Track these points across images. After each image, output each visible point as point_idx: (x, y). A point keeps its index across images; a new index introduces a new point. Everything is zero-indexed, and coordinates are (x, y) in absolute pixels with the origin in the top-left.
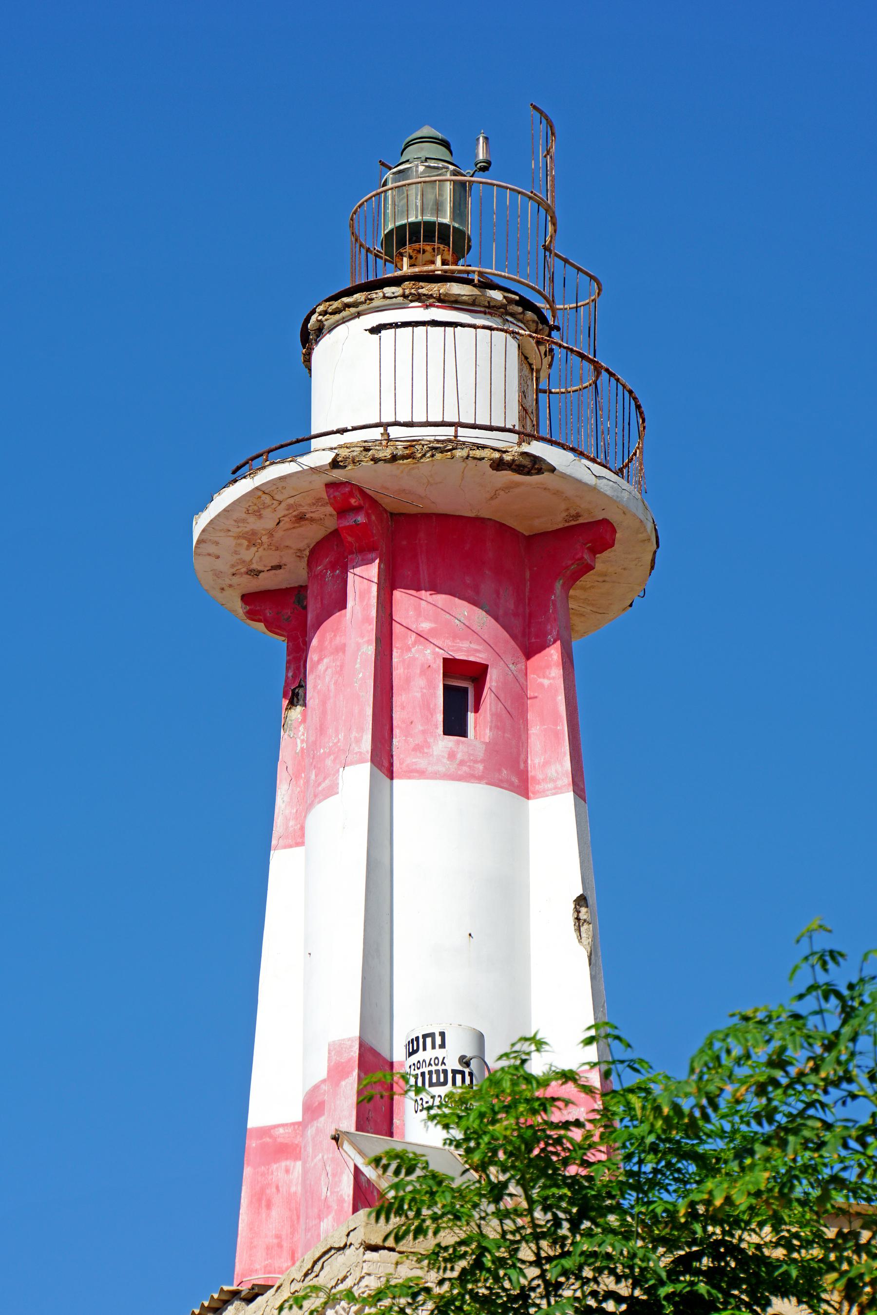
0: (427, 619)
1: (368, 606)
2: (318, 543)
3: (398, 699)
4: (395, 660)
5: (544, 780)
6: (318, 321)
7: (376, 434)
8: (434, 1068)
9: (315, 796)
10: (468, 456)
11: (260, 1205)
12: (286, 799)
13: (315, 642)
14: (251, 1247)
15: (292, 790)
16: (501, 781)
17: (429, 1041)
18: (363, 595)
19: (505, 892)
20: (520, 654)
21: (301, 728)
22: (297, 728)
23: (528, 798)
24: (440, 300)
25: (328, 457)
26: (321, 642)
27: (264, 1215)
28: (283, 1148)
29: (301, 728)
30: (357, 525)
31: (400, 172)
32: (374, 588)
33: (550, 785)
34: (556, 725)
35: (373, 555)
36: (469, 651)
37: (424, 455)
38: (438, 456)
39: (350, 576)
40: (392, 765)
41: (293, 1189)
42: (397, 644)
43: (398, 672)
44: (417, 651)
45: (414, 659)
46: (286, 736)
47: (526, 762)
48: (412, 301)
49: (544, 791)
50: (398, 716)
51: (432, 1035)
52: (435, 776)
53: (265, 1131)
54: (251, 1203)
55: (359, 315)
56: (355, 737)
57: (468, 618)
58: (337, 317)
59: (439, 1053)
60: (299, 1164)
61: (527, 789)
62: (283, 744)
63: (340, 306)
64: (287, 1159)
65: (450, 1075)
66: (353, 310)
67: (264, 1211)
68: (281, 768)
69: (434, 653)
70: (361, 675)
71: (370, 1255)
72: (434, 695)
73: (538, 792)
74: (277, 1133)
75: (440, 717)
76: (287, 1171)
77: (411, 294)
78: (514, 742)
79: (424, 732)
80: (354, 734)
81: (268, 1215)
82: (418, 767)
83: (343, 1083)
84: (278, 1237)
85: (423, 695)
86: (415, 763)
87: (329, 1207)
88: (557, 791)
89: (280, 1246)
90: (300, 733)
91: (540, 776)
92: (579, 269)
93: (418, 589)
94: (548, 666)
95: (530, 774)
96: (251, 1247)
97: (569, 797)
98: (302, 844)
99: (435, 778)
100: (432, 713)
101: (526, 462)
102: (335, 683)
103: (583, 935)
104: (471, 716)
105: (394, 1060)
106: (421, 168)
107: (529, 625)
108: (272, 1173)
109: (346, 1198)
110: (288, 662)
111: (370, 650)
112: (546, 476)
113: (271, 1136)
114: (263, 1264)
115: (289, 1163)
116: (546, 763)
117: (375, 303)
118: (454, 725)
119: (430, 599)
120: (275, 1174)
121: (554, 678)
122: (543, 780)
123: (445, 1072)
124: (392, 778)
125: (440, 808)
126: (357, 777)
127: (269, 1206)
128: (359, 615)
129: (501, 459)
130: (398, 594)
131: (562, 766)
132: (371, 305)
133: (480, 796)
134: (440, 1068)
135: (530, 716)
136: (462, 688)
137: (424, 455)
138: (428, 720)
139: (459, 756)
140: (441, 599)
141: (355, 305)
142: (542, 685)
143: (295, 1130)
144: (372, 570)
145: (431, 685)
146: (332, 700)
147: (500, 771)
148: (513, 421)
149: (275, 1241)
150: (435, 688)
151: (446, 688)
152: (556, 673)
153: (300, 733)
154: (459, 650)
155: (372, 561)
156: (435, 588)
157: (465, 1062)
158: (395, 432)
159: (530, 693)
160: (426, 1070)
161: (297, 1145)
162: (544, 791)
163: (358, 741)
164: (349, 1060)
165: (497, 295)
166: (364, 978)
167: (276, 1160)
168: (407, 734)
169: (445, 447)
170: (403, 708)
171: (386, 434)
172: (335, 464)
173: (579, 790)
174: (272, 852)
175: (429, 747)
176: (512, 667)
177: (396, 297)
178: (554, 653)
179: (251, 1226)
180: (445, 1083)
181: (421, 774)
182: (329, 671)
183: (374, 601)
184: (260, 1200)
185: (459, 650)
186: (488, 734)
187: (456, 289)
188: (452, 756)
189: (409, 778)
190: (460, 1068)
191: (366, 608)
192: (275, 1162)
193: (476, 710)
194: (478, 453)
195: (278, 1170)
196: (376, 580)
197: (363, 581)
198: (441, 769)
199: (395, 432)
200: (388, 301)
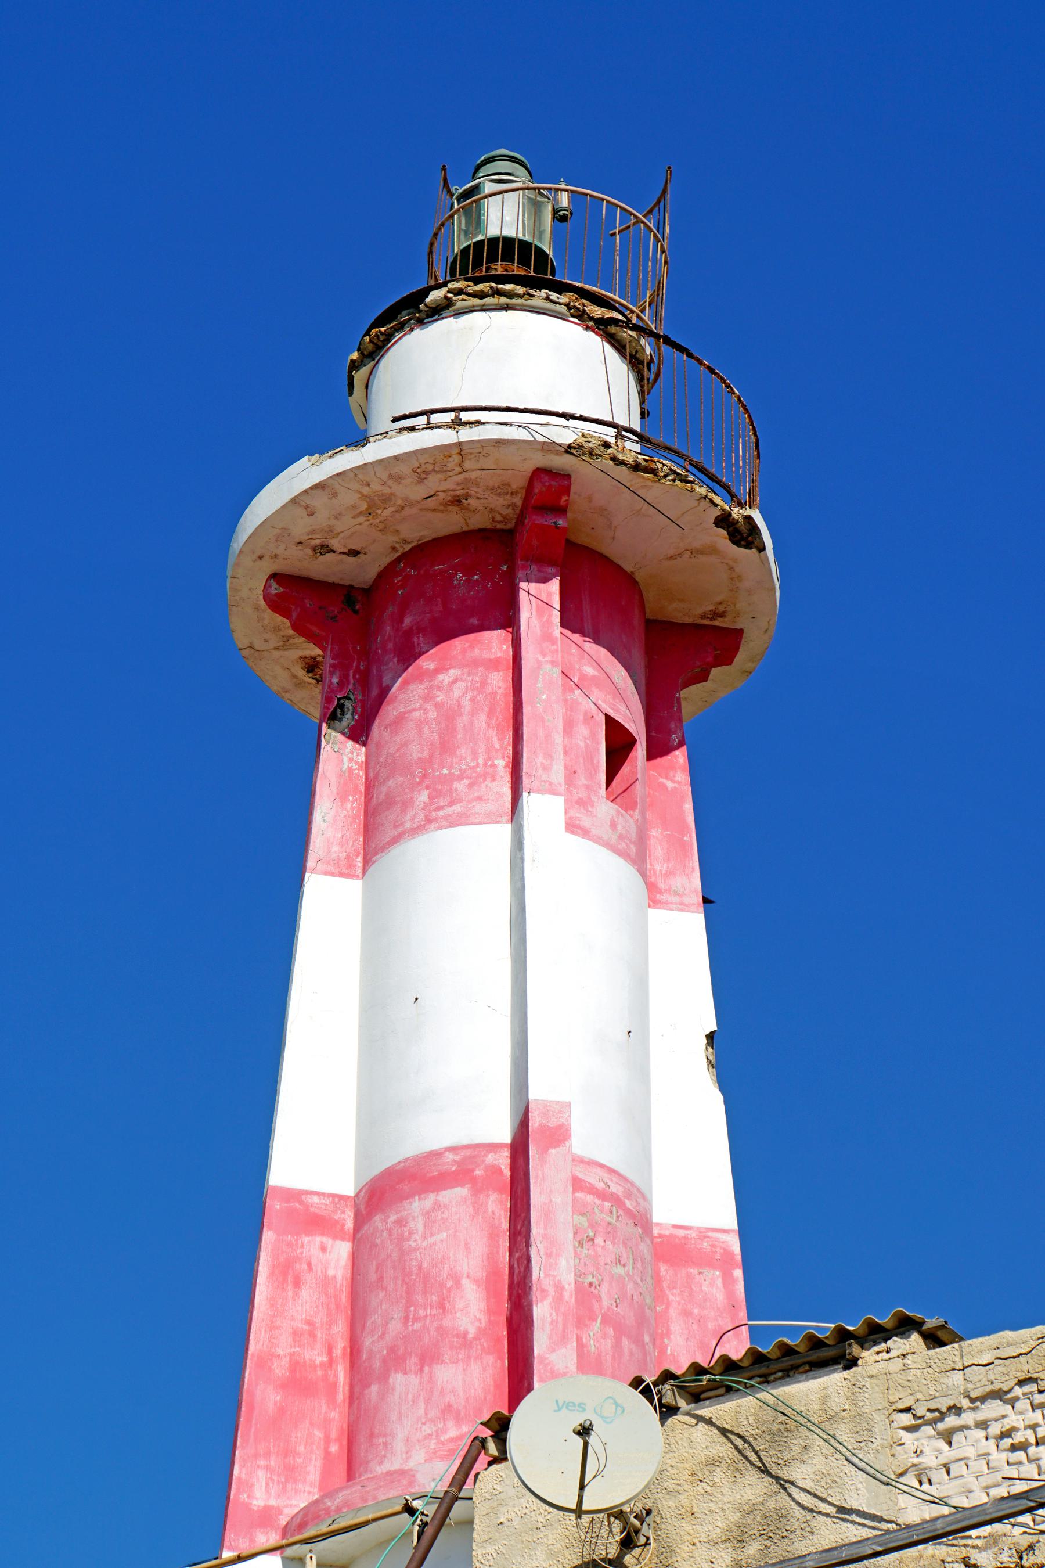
2: (435, 541)
5: (668, 890)
6: (446, 297)
10: (706, 496)
11: (285, 1281)
12: (329, 818)
15: (337, 812)
27: (290, 1294)
28: (311, 1217)
30: (557, 527)
33: (676, 899)
34: (684, 835)
35: (552, 570)
37: (665, 476)
38: (678, 483)
41: (331, 1272)
46: (328, 748)
48: (572, 316)
49: (667, 903)
52: (598, 840)
53: (292, 1195)
54: (271, 1275)
55: (507, 308)
56: (542, 763)
58: (477, 301)
63: (486, 290)
64: (323, 1234)
66: (504, 300)
70: (544, 697)
73: (659, 902)
74: (310, 1201)
76: (323, 1249)
77: (575, 307)
79: (588, 787)
81: (296, 1295)
82: (582, 824)
83: (553, 1151)
85: (587, 746)
88: (683, 907)
89: (312, 1335)
90: (347, 750)
93: (574, 631)
94: (673, 768)
96: (272, 1327)
99: (600, 844)
100: (596, 769)
101: (743, 527)
108: (302, 1247)
109: (567, 1286)
113: (301, 1202)
114: (288, 1351)
115: (327, 1241)
116: (669, 874)
117: (533, 302)
120: (306, 1247)
121: (679, 783)
122: (666, 890)
127: (297, 1283)
132: (529, 302)
137: (665, 476)
138: (591, 776)
141: (510, 295)
142: (665, 786)
143: (333, 1202)
145: (593, 736)
146: (465, 718)
149: (306, 1327)
153: (347, 750)
154: (617, 710)
155: (545, 580)
161: (337, 1222)
162: (667, 903)
167: (308, 1234)
169: (687, 476)
174: (307, 875)
177: (560, 304)
179: (272, 1302)
184: (285, 1274)
192: (307, 1235)
200: (550, 305)
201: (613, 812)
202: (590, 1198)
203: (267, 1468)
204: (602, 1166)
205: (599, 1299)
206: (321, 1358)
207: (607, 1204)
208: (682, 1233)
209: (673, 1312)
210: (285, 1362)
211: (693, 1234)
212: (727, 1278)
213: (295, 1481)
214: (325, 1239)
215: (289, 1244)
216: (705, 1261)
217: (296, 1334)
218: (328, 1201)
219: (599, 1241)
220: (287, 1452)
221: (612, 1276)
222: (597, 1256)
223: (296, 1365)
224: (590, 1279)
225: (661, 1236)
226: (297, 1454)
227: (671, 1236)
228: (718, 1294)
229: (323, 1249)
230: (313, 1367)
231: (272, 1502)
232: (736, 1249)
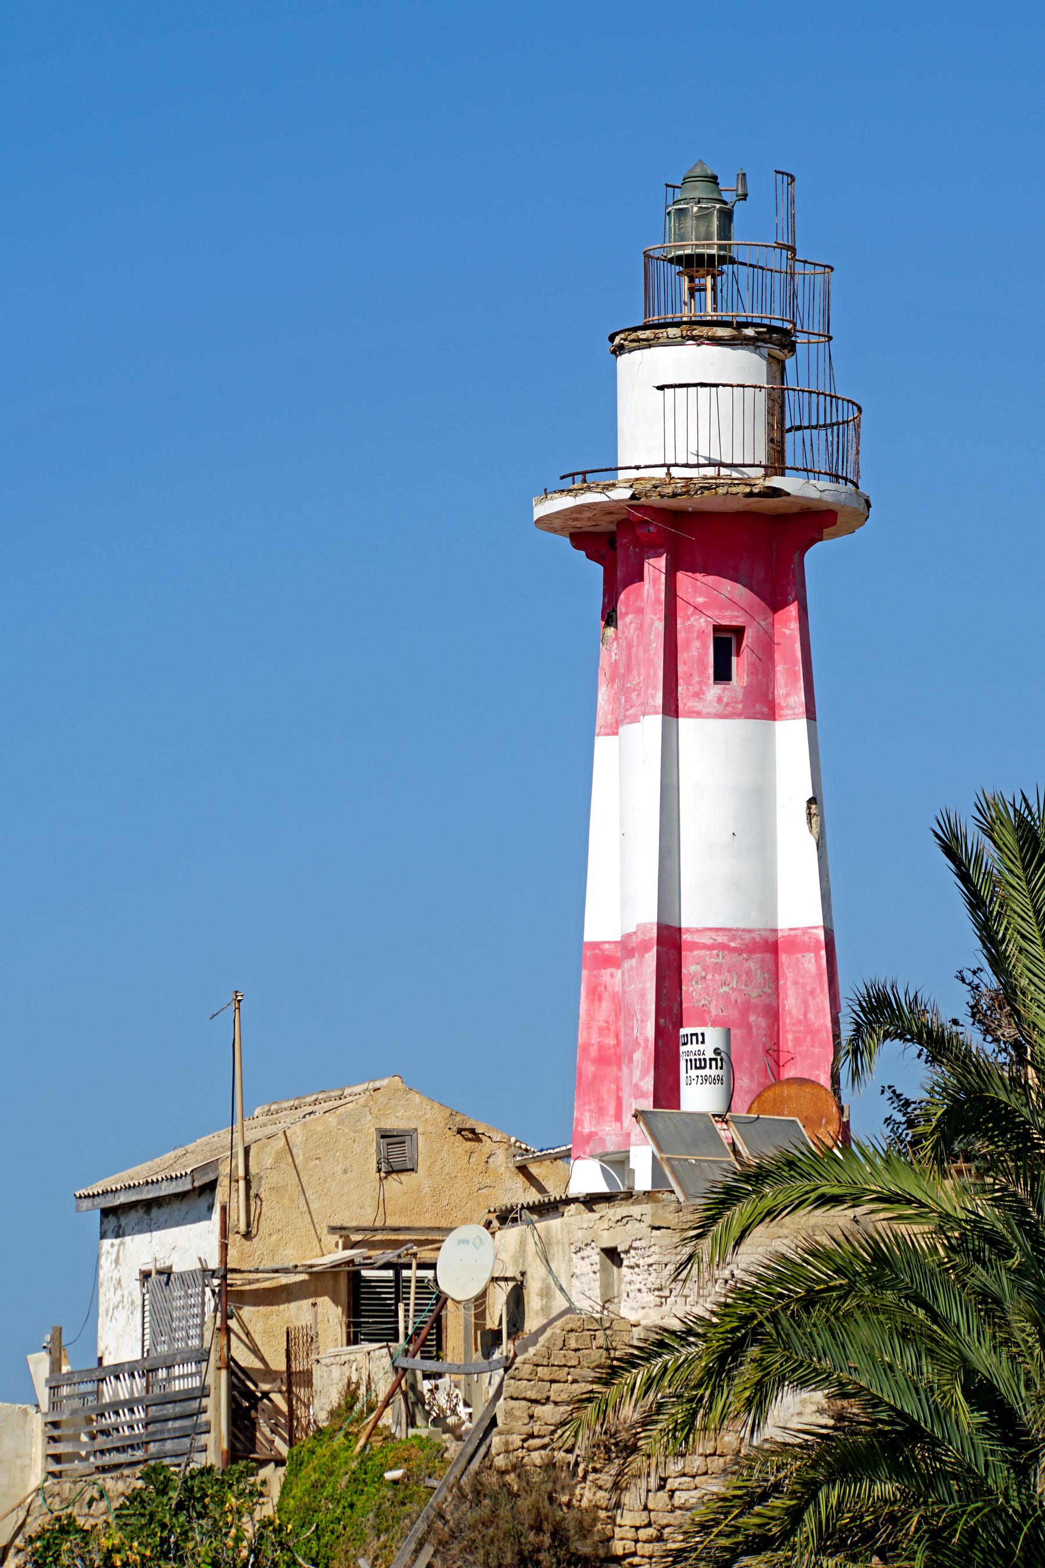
0: (701, 595)
1: (659, 589)
3: (682, 657)
4: (679, 626)
7: (661, 473)
8: (697, 1057)
13: (622, 596)
14: (589, 1028)
16: (755, 713)
17: (694, 1038)
18: (655, 581)
21: (615, 644)
22: (612, 644)
23: (775, 720)
24: (708, 339)
25: (627, 494)
26: (627, 598)
29: (615, 644)
31: (680, 209)
32: (663, 577)
33: (790, 712)
34: (795, 666)
35: (662, 550)
36: (732, 618)
38: (706, 493)
39: (646, 565)
40: (677, 706)
41: (616, 989)
43: (681, 636)
44: (695, 620)
45: (692, 626)
47: (773, 693)
50: (681, 669)
51: (696, 1035)
52: (709, 716)
53: (596, 945)
54: (587, 996)
55: (650, 346)
57: (730, 592)
59: (701, 1047)
60: (620, 971)
61: (774, 713)
62: (602, 655)
65: (708, 1062)
67: (596, 1002)
68: (601, 674)
69: (706, 621)
71: (655, 1233)
72: (707, 654)
75: (711, 671)
76: (612, 976)
78: (764, 681)
79: (700, 683)
80: (650, 691)
81: (600, 1006)
83: (647, 955)
84: (607, 1022)
85: (699, 654)
86: (694, 706)
87: (638, 1044)
88: (795, 716)
89: (608, 1029)
91: (783, 704)
92: (815, 264)
93: (694, 572)
94: (789, 620)
95: (777, 701)
96: (589, 1028)
98: (616, 734)
100: (706, 667)
101: (770, 491)
102: (638, 636)
103: (814, 826)
104: (734, 659)
105: (683, 926)
106: (695, 209)
107: (714, 1219)
111: (660, 626)
112: (784, 498)
113: (600, 949)
116: (788, 695)
117: (661, 341)
118: (722, 674)
119: (703, 579)
124: (677, 717)
125: (709, 741)
126: (654, 722)
127: (600, 999)
130: (680, 575)
133: (739, 729)
134: (702, 1057)
136: (726, 643)
139: (725, 700)
140: (711, 579)
142: (784, 633)
144: (662, 562)
145: (704, 647)
147: (754, 706)
148: (762, 458)
150: (707, 648)
152: (795, 625)
155: (660, 556)
157: (717, 1051)
158: (676, 472)
159: (776, 640)
160: (693, 1058)
163: (653, 696)
164: (651, 939)
165: (750, 332)
166: (660, 878)
167: (605, 968)
170: (685, 664)
171: (668, 474)
172: (633, 497)
173: (811, 714)
175: (704, 694)
176: (763, 623)
178: (793, 610)
181: (698, 714)
182: (633, 625)
185: (724, 617)
188: (720, 700)
189: (690, 717)
190: (714, 1056)
193: (738, 655)
194: (734, 490)
195: (606, 974)
196: (664, 570)
198: (713, 710)
199: (676, 472)
201: (719, 691)
202: (702, 953)
203: (590, 1110)
204: (711, 929)
205: (709, 1012)
206: (613, 1042)
207: (714, 952)
208: (793, 933)
209: (789, 983)
210: (596, 1047)
211: (799, 932)
212: (818, 957)
214: (612, 970)
215: (596, 976)
216: (805, 948)
217: (600, 1029)
218: (613, 946)
219: (710, 977)
220: (599, 1100)
221: (718, 995)
222: (708, 987)
223: (601, 1048)
224: (703, 1002)
225: (783, 937)
226: (603, 1100)
227: (789, 936)
229: (612, 976)
230: (610, 1048)
231: (593, 1129)
232: (822, 938)
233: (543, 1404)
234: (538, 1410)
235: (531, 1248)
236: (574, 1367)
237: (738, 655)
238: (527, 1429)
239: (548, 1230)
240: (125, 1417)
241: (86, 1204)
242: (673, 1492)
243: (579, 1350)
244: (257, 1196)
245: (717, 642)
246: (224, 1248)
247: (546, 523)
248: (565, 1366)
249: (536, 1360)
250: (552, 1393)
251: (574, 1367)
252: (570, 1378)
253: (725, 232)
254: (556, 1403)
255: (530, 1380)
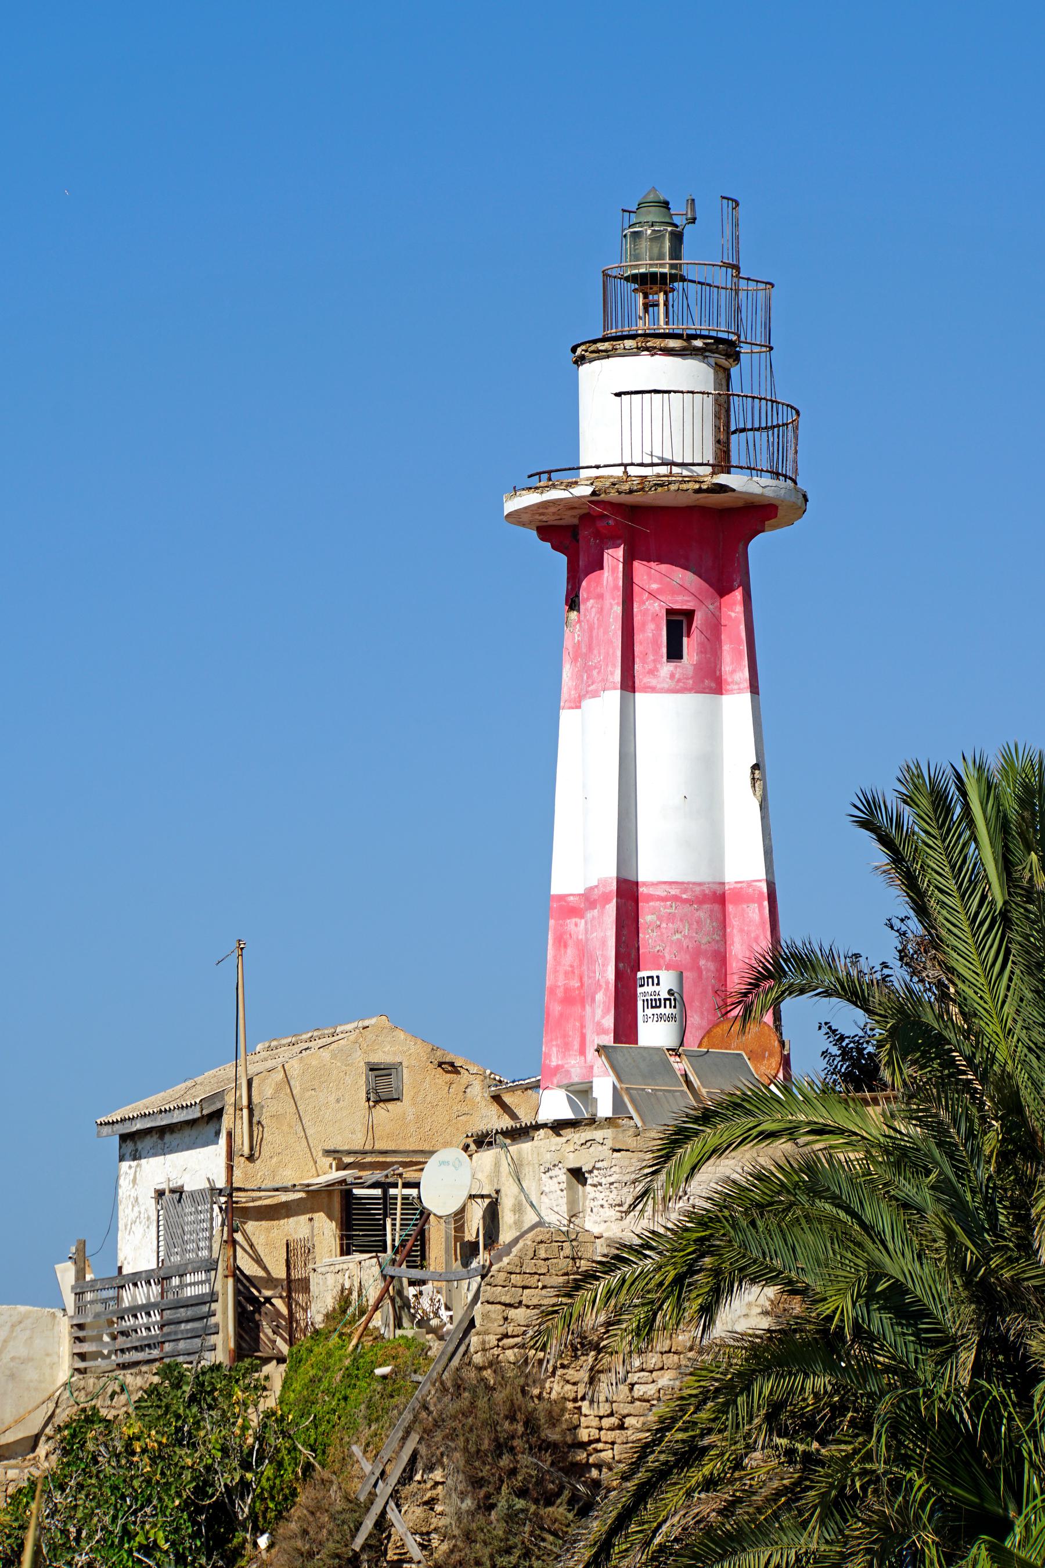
0: (655, 582)
1: (617, 577)
3: (638, 637)
7: (619, 472)
9: (587, 692)
13: (584, 584)
14: (556, 971)
18: (614, 570)
19: (707, 764)
20: (716, 595)
21: (578, 626)
22: (575, 626)
24: (661, 350)
26: (589, 584)
29: (578, 626)
32: (621, 565)
33: (736, 687)
35: (619, 542)
38: (660, 489)
39: (605, 555)
41: (580, 937)
42: (636, 599)
43: (637, 619)
45: (647, 610)
47: (720, 670)
50: (638, 649)
51: (652, 977)
52: (663, 691)
53: (562, 898)
54: (554, 942)
55: (608, 357)
59: (656, 988)
60: (583, 921)
69: (660, 605)
71: (616, 1154)
72: (660, 635)
75: (664, 650)
76: (576, 925)
79: (654, 661)
80: (610, 668)
81: (565, 952)
84: (572, 966)
88: (740, 691)
89: (573, 972)
91: (730, 680)
93: (649, 561)
94: (734, 604)
96: (556, 971)
97: (747, 696)
98: (579, 707)
100: (660, 647)
104: (685, 639)
110: (568, 578)
111: (618, 610)
115: (578, 920)
116: (733, 672)
117: (618, 352)
118: (675, 653)
123: (660, 1000)
126: (613, 697)
127: (565, 946)
128: (611, 584)
129: (700, 488)
130: (636, 564)
131: (744, 675)
133: (691, 701)
135: (723, 637)
136: (678, 624)
138: (656, 652)
139: (677, 676)
140: (664, 568)
142: (730, 616)
144: (619, 552)
147: (703, 682)
148: (710, 458)
150: (661, 630)
151: (668, 621)
152: (739, 609)
155: (618, 546)
156: (661, 561)
157: (670, 992)
158: (633, 471)
159: (723, 622)
163: (612, 674)
165: (698, 343)
168: (644, 662)
171: (625, 472)
172: (594, 493)
173: (754, 689)
176: (711, 607)
178: (738, 595)
179: (555, 957)
180: (660, 1007)
181: (653, 690)
183: (621, 575)
184: (560, 942)
185: (676, 602)
186: (695, 658)
187: (672, 343)
191: (615, 579)
193: (688, 636)
194: (684, 486)
195: (571, 923)
196: (621, 560)
197: (614, 557)
198: (666, 686)
199: (633, 471)
201: (671, 668)
202: (657, 904)
203: (557, 1046)
207: (668, 903)
208: (739, 885)
209: (735, 931)
210: (562, 989)
211: (744, 885)
212: (761, 906)
213: (569, 1050)
215: (561, 925)
216: (750, 899)
217: (566, 973)
219: (664, 925)
220: (565, 1036)
223: (567, 990)
224: (658, 948)
228: (756, 917)
229: (576, 925)
231: (560, 1063)
232: (765, 890)
233: (516, 1308)
234: (512, 1313)
235: (505, 1169)
236: (544, 1274)
237: (688, 636)
238: (502, 1330)
239: (519, 1152)
240: (142, 1319)
241: (106, 1130)
242: (633, 1385)
243: (548, 1259)
244: (259, 1123)
245: (669, 623)
246: (230, 1169)
247: (515, 517)
248: (535, 1273)
249: (509, 1268)
250: (524, 1298)
251: (544, 1274)
252: (540, 1284)
253: (676, 253)
254: (528, 1307)
255: (504, 1287)
